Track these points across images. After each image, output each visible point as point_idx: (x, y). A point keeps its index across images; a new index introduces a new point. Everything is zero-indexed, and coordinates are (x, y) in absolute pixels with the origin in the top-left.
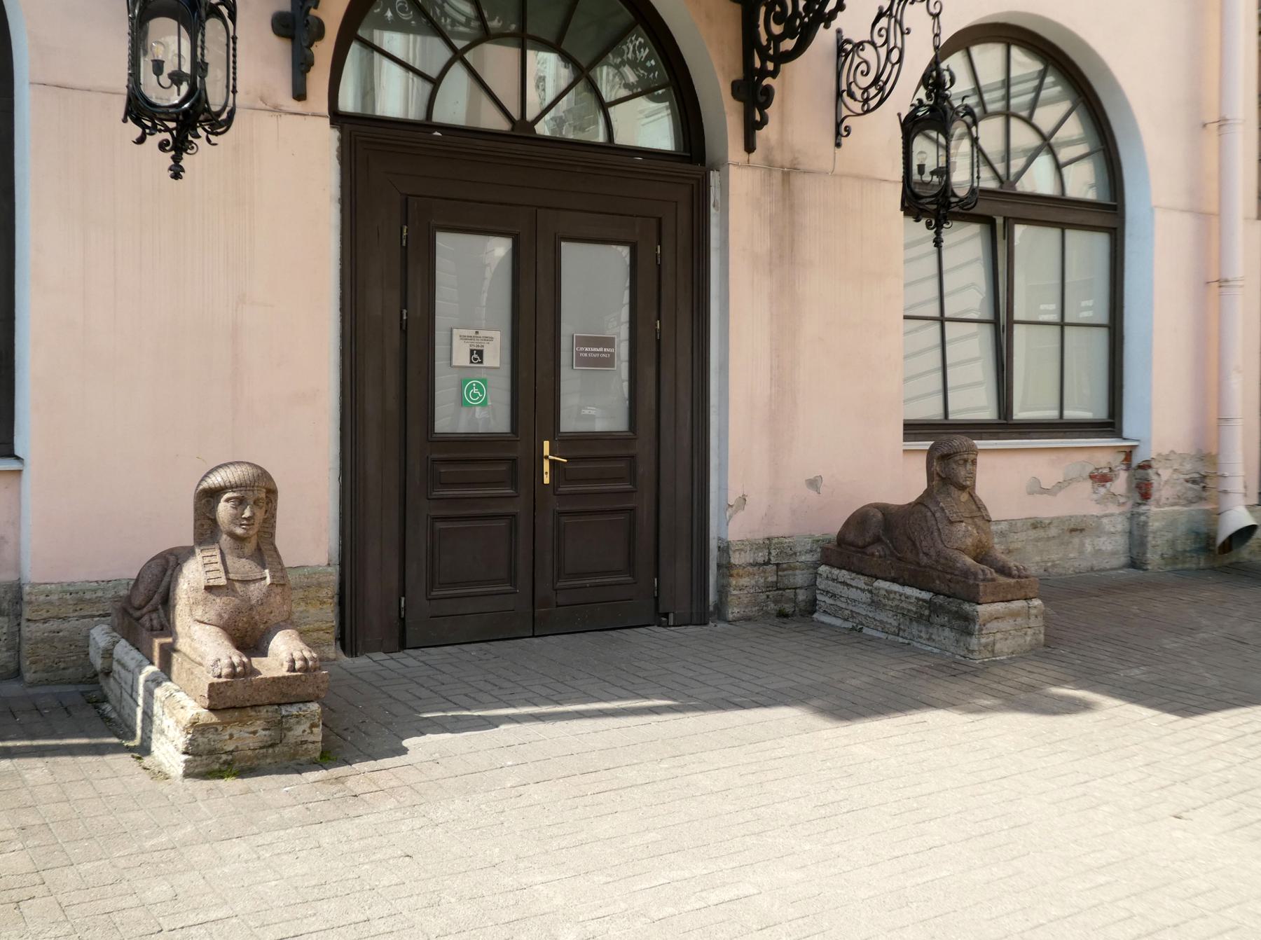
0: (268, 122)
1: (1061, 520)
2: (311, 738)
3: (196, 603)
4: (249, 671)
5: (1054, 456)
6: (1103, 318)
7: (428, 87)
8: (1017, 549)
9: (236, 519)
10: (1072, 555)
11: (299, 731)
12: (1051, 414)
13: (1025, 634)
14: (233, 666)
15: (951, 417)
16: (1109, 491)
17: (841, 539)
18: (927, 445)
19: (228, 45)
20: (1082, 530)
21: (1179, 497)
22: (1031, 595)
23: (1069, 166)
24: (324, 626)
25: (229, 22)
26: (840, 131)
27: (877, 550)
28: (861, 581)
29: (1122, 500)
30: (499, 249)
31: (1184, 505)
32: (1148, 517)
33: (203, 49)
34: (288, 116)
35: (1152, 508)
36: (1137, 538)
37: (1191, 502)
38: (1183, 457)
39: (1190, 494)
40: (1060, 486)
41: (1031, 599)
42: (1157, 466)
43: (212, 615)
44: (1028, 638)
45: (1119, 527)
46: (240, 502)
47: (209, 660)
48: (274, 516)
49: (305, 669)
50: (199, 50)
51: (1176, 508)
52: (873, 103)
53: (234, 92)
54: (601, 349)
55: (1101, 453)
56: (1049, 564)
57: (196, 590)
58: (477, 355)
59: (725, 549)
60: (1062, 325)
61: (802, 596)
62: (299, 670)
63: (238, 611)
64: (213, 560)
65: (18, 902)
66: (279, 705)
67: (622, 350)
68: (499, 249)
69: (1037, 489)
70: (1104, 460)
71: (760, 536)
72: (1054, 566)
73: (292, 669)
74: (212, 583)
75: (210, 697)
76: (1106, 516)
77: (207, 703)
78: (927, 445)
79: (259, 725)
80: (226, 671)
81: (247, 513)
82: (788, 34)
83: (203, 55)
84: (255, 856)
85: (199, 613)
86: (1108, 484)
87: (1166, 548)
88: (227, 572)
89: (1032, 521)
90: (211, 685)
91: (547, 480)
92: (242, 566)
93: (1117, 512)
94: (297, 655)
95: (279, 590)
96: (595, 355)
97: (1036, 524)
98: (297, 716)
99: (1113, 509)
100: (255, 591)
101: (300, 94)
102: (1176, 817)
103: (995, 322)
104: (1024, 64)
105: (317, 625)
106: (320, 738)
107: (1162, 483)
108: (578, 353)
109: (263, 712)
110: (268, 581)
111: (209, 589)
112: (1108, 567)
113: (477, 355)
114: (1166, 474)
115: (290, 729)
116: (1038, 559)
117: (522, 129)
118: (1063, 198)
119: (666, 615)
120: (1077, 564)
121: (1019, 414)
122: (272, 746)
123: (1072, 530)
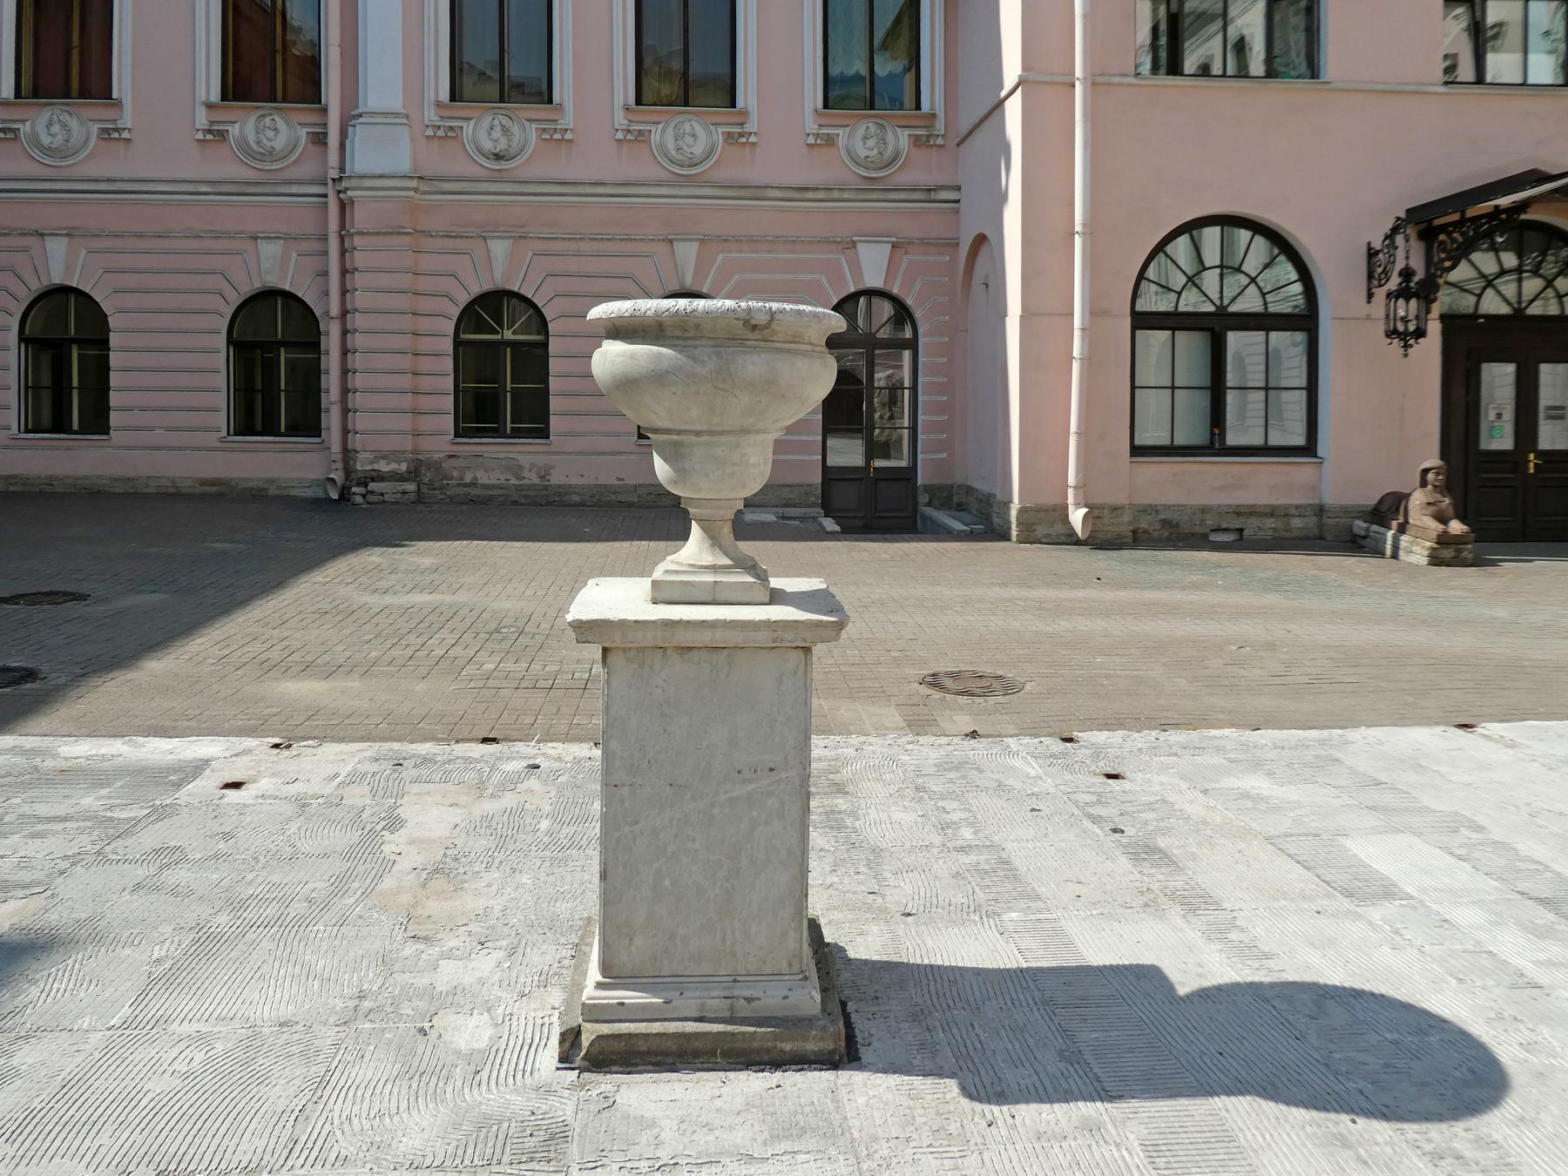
6: (1303, 382)
11: (1465, 554)
12: (1165, 441)
15: (1175, 443)
30: (1510, 368)
43: (1429, 512)
52: (1383, 281)
58: (1499, 416)
60: (1173, 388)
65: (1524, 84)
67: (1541, 415)
68: (1510, 368)
102: (1109, 776)
111: (1429, 504)
113: (1499, 416)
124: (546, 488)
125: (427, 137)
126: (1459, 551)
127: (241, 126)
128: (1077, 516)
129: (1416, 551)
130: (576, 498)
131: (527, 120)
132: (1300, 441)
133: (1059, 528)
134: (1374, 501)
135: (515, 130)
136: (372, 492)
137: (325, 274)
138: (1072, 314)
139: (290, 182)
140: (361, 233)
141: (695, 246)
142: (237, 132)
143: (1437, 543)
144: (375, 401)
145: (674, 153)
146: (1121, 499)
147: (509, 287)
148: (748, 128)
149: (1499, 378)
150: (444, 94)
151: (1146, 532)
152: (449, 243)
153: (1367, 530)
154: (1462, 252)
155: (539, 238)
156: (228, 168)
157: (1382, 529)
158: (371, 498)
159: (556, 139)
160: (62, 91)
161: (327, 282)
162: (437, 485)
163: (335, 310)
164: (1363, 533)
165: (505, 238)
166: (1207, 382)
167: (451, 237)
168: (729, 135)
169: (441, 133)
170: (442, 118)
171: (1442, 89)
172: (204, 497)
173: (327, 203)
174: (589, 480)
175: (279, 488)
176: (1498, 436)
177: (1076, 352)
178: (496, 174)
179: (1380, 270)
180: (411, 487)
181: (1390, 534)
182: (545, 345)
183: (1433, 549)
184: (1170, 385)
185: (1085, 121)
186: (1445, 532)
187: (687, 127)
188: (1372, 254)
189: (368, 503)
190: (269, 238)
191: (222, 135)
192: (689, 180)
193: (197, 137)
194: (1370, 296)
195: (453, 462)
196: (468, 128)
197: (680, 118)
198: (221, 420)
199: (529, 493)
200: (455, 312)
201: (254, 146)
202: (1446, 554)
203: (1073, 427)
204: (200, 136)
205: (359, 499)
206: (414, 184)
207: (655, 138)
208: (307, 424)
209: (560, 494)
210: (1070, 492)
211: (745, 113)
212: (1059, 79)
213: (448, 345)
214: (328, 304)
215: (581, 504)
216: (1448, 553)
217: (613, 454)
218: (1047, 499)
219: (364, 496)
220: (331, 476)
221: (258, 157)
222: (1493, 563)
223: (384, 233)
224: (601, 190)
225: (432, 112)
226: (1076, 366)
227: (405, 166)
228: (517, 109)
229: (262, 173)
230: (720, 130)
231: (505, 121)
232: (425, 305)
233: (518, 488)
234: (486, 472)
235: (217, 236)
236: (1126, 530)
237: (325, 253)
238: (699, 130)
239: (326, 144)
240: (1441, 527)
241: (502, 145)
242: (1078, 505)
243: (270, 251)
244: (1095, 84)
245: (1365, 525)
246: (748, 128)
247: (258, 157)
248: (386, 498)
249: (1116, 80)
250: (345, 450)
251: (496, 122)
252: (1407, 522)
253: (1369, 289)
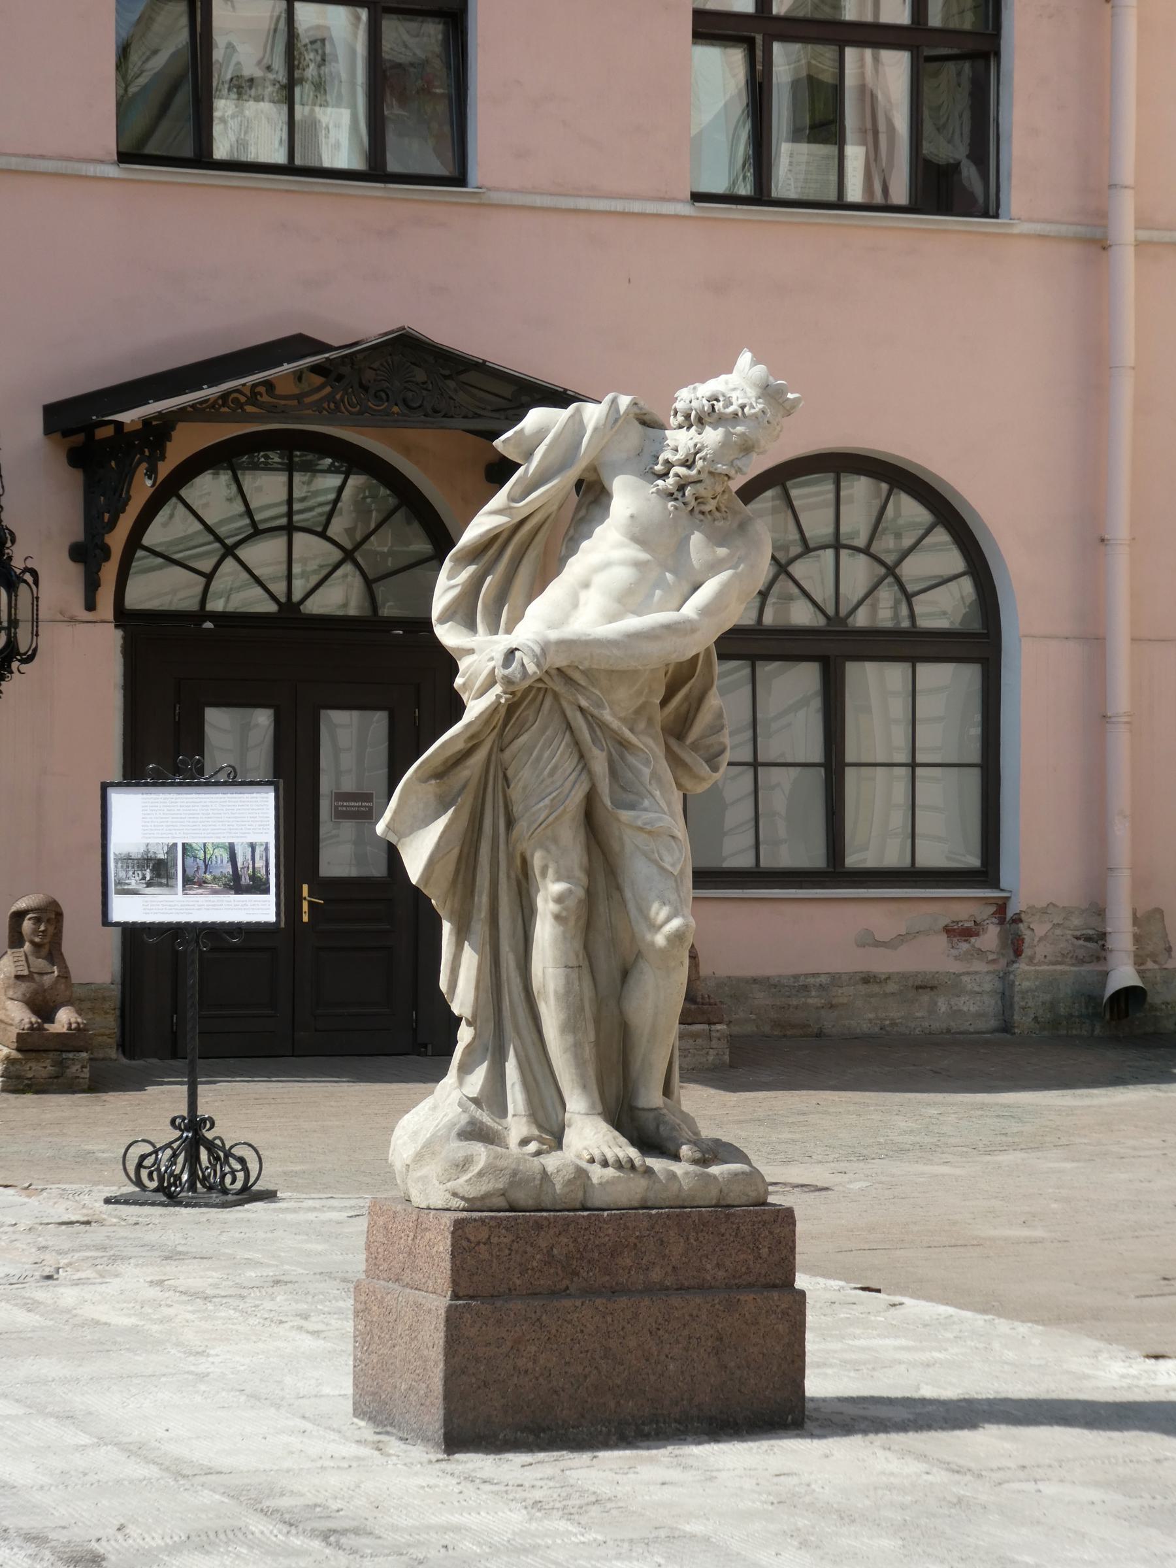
0: (67, 630)
1: (904, 976)
2: (82, 1075)
3: (9, 987)
4: (40, 1028)
5: (893, 906)
7: (202, 580)
8: (843, 1004)
9: (35, 932)
10: (919, 1015)
11: (74, 1069)
13: (707, 1053)
14: (31, 1023)
15: (763, 864)
16: (973, 946)
19: (33, 604)
20: (932, 988)
21: (1063, 955)
22: (715, 1020)
24: (107, 1032)
25: (34, 587)
29: (991, 957)
31: (1073, 965)
32: (1015, 976)
33: (16, 610)
34: (82, 625)
35: (1022, 966)
36: (1006, 996)
37: (1082, 962)
38: (1068, 912)
39: (1081, 953)
40: (902, 939)
41: (714, 1024)
42: (1030, 920)
43: (19, 995)
44: (711, 1058)
45: (987, 987)
46: (38, 921)
47: (17, 1020)
48: (60, 931)
49: (78, 1029)
50: (13, 610)
51: (1059, 967)
53: (37, 635)
54: (360, 804)
56: (887, 1022)
57: (9, 978)
60: (913, 765)
62: (74, 1029)
63: (36, 993)
64: (20, 959)
65: (289, 169)
66: (62, 1051)
68: (263, 719)
69: (869, 941)
72: (893, 1024)
73: (70, 1028)
74: (19, 973)
75: (17, 1042)
76: (968, 973)
77: (15, 1045)
79: (48, 1063)
80: (27, 1026)
81: (42, 928)
83: (15, 614)
85: (10, 993)
86: (973, 940)
87: (1041, 1011)
88: (29, 967)
90: (18, 1034)
91: (305, 918)
92: (40, 964)
93: (986, 970)
94: (73, 1020)
95: (63, 980)
96: (353, 809)
97: (868, 979)
98: (73, 1059)
99: (980, 966)
100: (47, 980)
101: (90, 606)
105: (102, 1031)
106: (87, 1076)
107: (1037, 939)
108: (336, 807)
109: (51, 1055)
110: (56, 974)
111: (18, 977)
112: (972, 1030)
114: (1041, 929)
115: (68, 1067)
116: (871, 1016)
117: (289, 609)
118: (914, 630)
119: (425, 1046)
120: (927, 1024)
121: (853, 860)
122: (57, 1077)
123: (918, 988)
126: (61, 1065)
132: (973, 861)
143: (18, 1050)
166: (975, 756)
171: (113, 171)
184: (760, 759)
216: (41, 1069)
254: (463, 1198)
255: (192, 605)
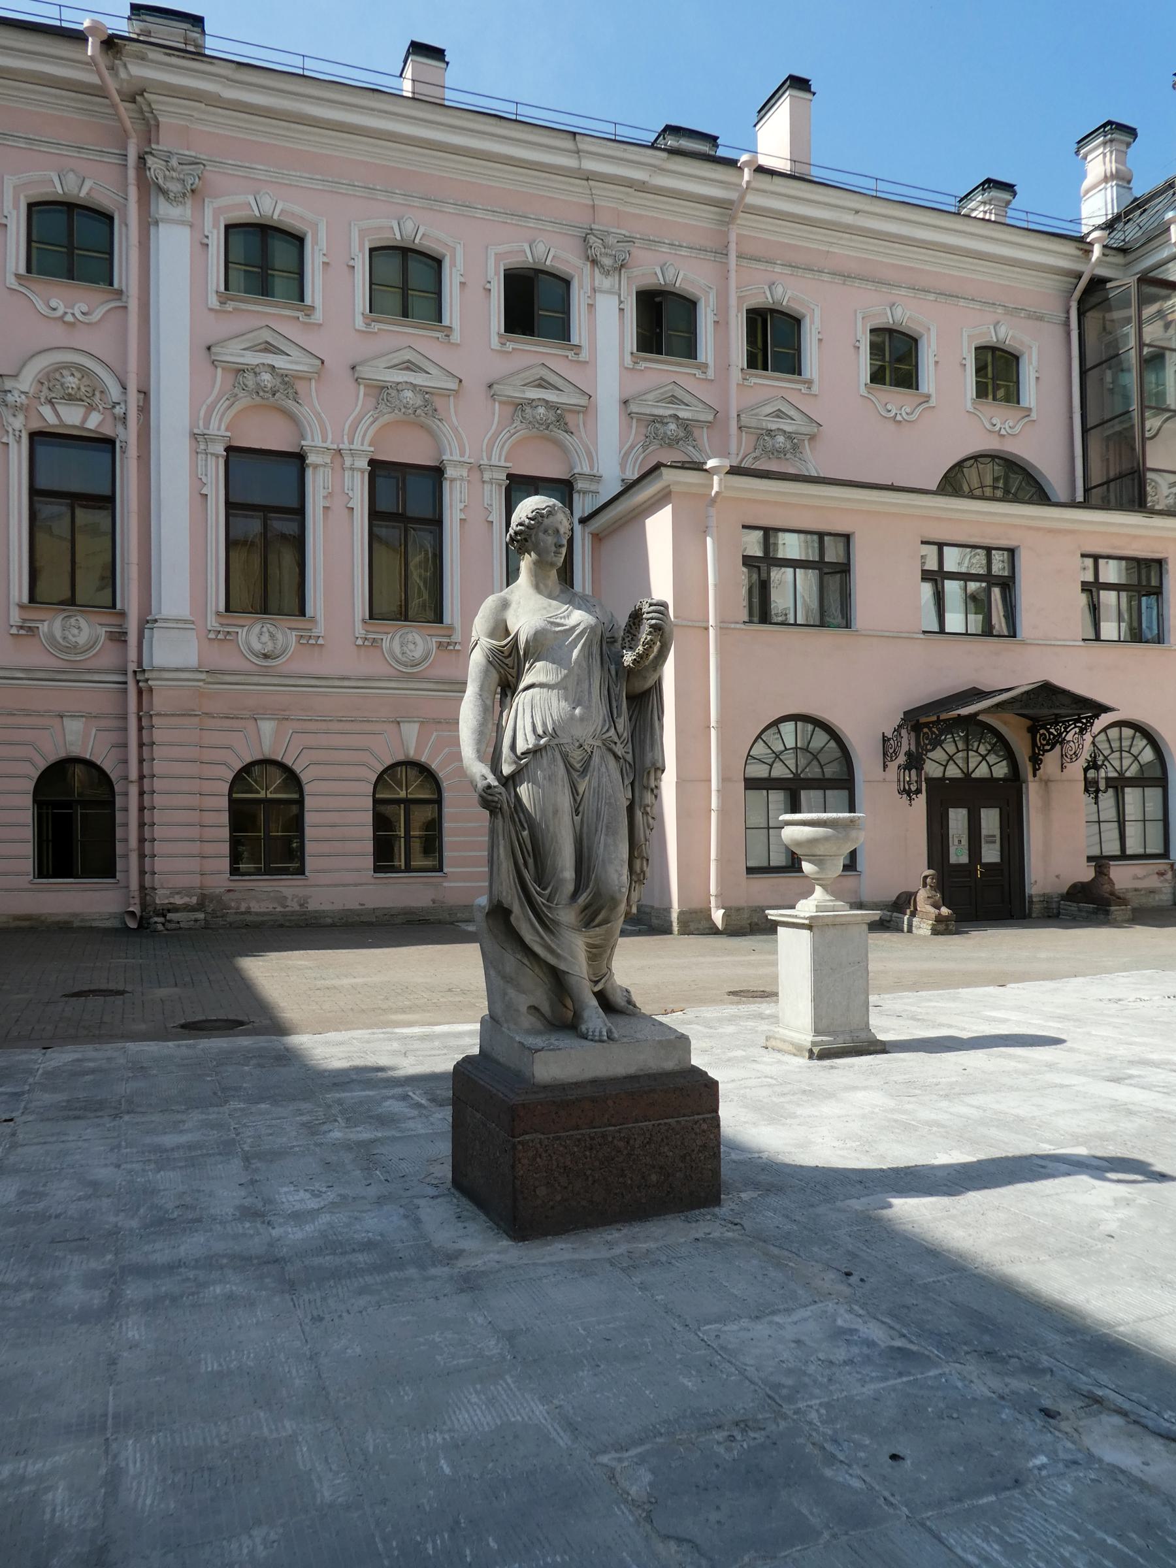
1: (1145, 889)
6: (1160, 816)
11: (951, 927)
17: (1068, 893)
18: (1094, 864)
23: (922, 1055)
26: (1063, 768)
27: (1079, 895)
28: (1075, 905)
55: (1161, 864)
59: (1031, 897)
60: (1144, 821)
61: (1055, 911)
69: (1136, 878)
70: (1162, 868)
71: (1041, 892)
78: (1094, 864)
82: (1048, 744)
84: (206, 1474)
89: (129, 436)
97: (1136, 890)
99: (1167, 885)
103: (1119, 821)
104: (1127, 732)
124: (304, 913)
125: (209, 639)
126: (947, 925)
127: (49, 625)
128: (718, 916)
129: (923, 927)
130: (329, 921)
131: (289, 629)
133: (704, 924)
134: (894, 899)
135: (279, 636)
136: (169, 921)
137: (125, 746)
138: (710, 781)
139: (89, 671)
140: (158, 715)
141: (416, 726)
142: (46, 629)
144: (324, 848)
145: (400, 656)
146: (742, 903)
147: (274, 757)
148: (455, 638)
149: (958, 819)
150: (222, 607)
151: (757, 924)
152: (227, 723)
153: (891, 916)
154: (937, 743)
155: (299, 720)
156: (34, 656)
157: (900, 915)
158: (169, 926)
159: (310, 642)
160: (403, 615)
161: (126, 754)
162: (219, 914)
163: (134, 775)
164: (888, 919)
165: (273, 719)
167: (227, 718)
168: (440, 644)
169: (220, 636)
170: (222, 625)
172: (18, 930)
173: (126, 689)
174: (338, 906)
175: (82, 920)
176: (958, 854)
177: (714, 805)
178: (265, 670)
179: (891, 751)
180: (201, 916)
181: (906, 918)
182: (300, 802)
183: (933, 924)
185: (716, 650)
186: (939, 914)
187: (410, 637)
188: (885, 740)
189: (167, 930)
190: (75, 716)
191: (32, 631)
192: (411, 677)
193: (12, 632)
194: (885, 767)
195: (231, 895)
196: (242, 633)
197: (407, 629)
198: (29, 865)
199: (293, 918)
200: (230, 776)
201: (61, 641)
202: (942, 928)
203: (713, 855)
204: (14, 631)
205: (160, 927)
206: (203, 676)
207: (385, 645)
208: (104, 867)
209: (316, 918)
210: (713, 899)
211: (451, 628)
212: (697, 624)
213: (224, 803)
214: (127, 769)
215: (333, 925)
216: (941, 927)
217: (356, 885)
218: (696, 904)
219: (163, 925)
220: (131, 909)
221: (65, 650)
222: (967, 932)
223: (179, 715)
224: (346, 683)
225: (360, 627)
226: (714, 815)
227: (193, 661)
228: (280, 619)
229: (254, 666)
230: (434, 640)
231: (272, 629)
232: (208, 771)
233: (284, 914)
234: (258, 902)
235: (28, 713)
236: (745, 923)
237: (125, 729)
238: (418, 639)
239: (126, 641)
240: (937, 911)
241: (269, 647)
242: (718, 908)
243: (74, 727)
244: (723, 627)
245: (889, 913)
246: (455, 638)
247: (65, 650)
248: (182, 925)
249: (733, 626)
250: (142, 887)
251: (265, 629)
252: (916, 909)
253: (884, 763)
254: (874, 906)
255: (940, 775)
